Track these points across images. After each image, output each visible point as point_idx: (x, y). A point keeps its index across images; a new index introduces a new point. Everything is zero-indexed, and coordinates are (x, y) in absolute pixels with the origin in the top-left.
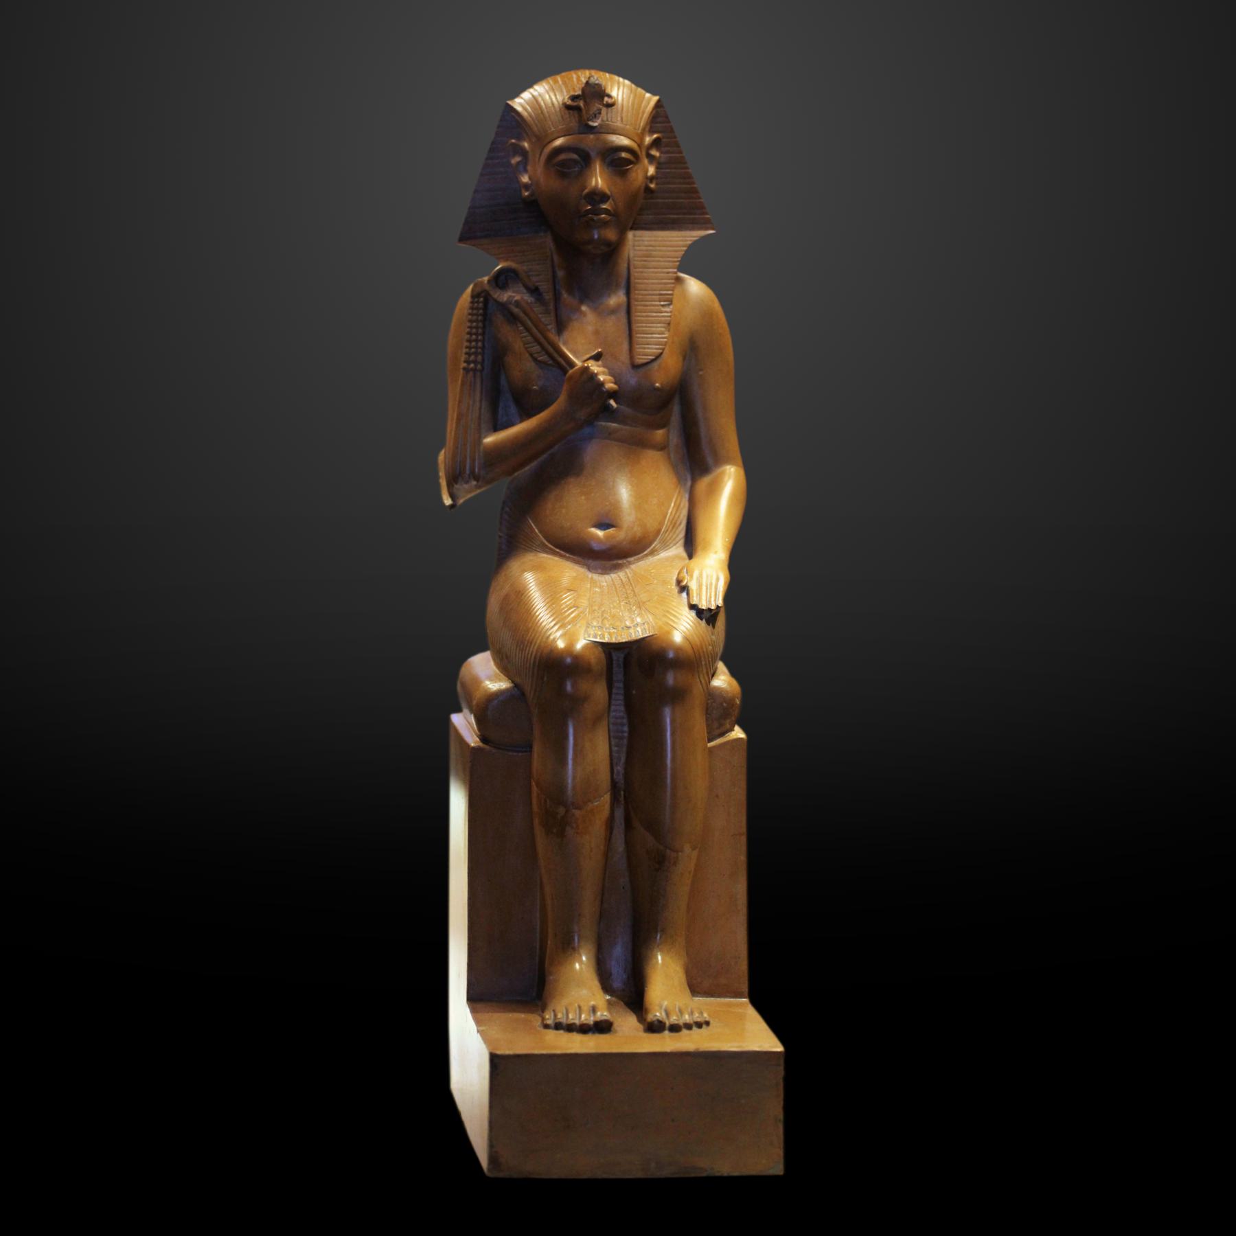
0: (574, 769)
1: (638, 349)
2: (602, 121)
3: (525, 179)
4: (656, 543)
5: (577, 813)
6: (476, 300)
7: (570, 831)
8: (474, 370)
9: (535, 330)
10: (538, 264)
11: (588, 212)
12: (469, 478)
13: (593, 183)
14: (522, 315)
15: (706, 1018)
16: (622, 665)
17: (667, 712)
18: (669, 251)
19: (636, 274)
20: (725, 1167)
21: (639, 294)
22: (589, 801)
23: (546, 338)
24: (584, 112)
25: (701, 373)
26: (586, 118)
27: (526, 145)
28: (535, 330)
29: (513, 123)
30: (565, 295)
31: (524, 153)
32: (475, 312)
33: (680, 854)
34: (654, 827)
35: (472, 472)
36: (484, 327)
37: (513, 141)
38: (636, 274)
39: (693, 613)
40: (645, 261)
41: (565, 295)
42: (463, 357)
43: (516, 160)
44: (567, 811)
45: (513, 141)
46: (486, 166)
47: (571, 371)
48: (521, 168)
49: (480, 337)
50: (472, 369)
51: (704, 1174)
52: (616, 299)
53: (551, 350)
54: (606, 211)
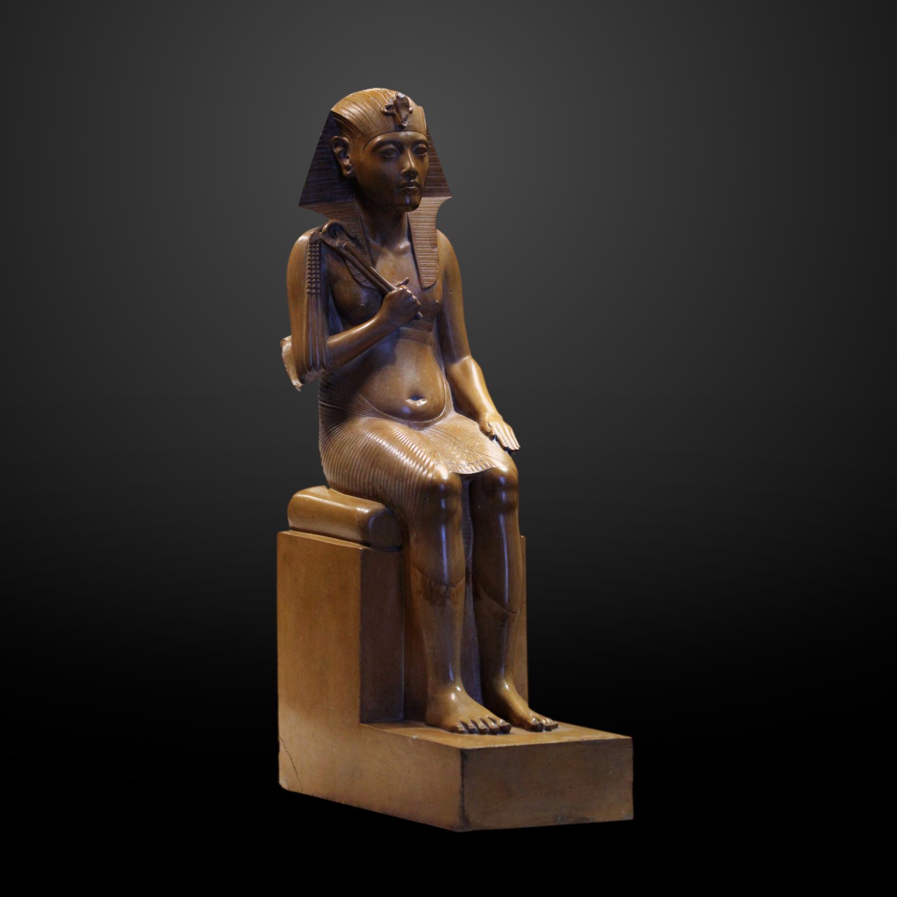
0: (448, 561)
1: (424, 277)
2: (408, 123)
3: (347, 162)
4: (444, 409)
5: (453, 589)
6: (314, 245)
7: (448, 602)
8: (316, 294)
9: (361, 266)
10: (353, 221)
11: (405, 185)
12: (320, 367)
13: (408, 165)
14: (350, 255)
15: (532, 720)
16: (468, 490)
17: (502, 519)
18: (429, 211)
19: (414, 227)
20: (600, 817)
21: (417, 240)
22: (459, 581)
24: (398, 116)
25: (451, 293)
26: (401, 121)
27: (346, 139)
28: (361, 266)
29: (338, 124)
30: (372, 241)
31: (345, 146)
32: (313, 254)
33: (516, 614)
35: (322, 363)
37: (336, 137)
38: (414, 227)
39: (506, 453)
40: (417, 218)
41: (372, 241)
42: (307, 285)
43: (338, 150)
44: (447, 589)
45: (336, 137)
46: (316, 154)
47: (390, 293)
48: (342, 155)
49: (318, 271)
50: (314, 293)
51: (589, 822)
52: (404, 244)
53: (373, 278)
54: (415, 184)
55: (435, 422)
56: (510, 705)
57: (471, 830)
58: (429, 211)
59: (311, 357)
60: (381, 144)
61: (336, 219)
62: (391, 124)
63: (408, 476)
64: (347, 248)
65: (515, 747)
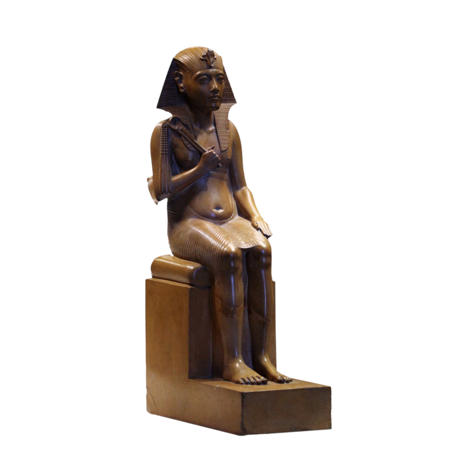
0: (235, 294)
1: (222, 145)
2: (214, 64)
3: (182, 85)
4: (233, 214)
5: (237, 309)
6: (164, 129)
7: (235, 316)
8: (166, 154)
9: (189, 139)
10: (185, 116)
11: (212, 97)
12: (168, 192)
13: (214, 87)
14: (183, 134)
15: (279, 377)
16: (245, 257)
17: (263, 272)
18: (225, 110)
19: (217, 119)
21: (219, 126)
22: (240, 304)
24: (208, 61)
25: (236, 154)
26: (210, 64)
27: (181, 73)
28: (189, 139)
30: (195, 126)
31: (181, 76)
32: (164, 133)
33: (270, 322)
34: (261, 313)
35: (169, 190)
36: (168, 139)
37: (176, 72)
38: (217, 119)
39: (265, 237)
40: (219, 114)
41: (195, 126)
42: (161, 149)
43: (177, 79)
44: (234, 308)
45: (176, 72)
47: (204, 154)
48: (179, 81)
49: (167, 142)
50: (165, 154)
52: (212, 128)
53: (196, 146)
54: (218, 96)
55: (228, 221)
56: (267, 369)
58: (225, 110)
59: (163, 187)
60: (200, 75)
61: (176, 115)
62: (205, 65)
63: (214, 249)
64: (182, 130)
65: (270, 391)
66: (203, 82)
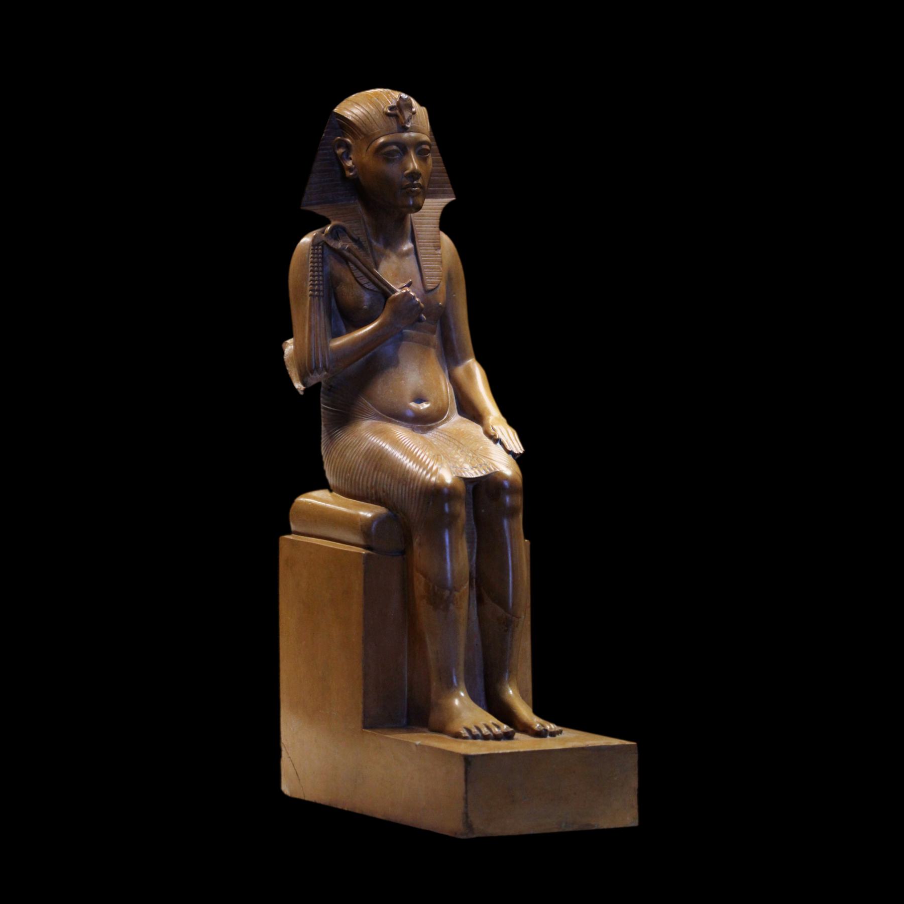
0: (452, 566)
1: (427, 280)
2: (412, 124)
3: (350, 163)
4: (448, 412)
5: (457, 594)
6: (316, 247)
7: (452, 607)
8: (319, 296)
9: (363, 268)
10: (356, 222)
11: (408, 186)
12: (323, 370)
13: (411, 167)
14: (353, 257)
16: (471, 494)
17: (506, 523)
18: (433, 212)
19: (417, 228)
20: (605, 823)
21: (421, 242)
22: (462, 585)
23: (373, 273)
24: (401, 117)
25: (454, 295)
26: (404, 122)
27: (348, 140)
28: (363, 268)
30: (375, 243)
31: (348, 147)
32: (316, 256)
33: (520, 619)
35: (324, 366)
37: (339, 138)
38: (417, 228)
39: (510, 457)
40: (421, 219)
41: (375, 243)
42: (309, 287)
43: (340, 151)
44: (451, 593)
45: (339, 138)
47: (393, 295)
48: (344, 156)
49: (320, 273)
50: (317, 296)
51: (594, 828)
52: (408, 246)
53: (376, 280)
54: (419, 185)
55: (438, 425)
56: (514, 711)
57: (474, 836)
58: (433, 212)
59: (313, 360)
60: (384, 145)
61: (339, 220)
62: (394, 125)
63: (411, 480)
64: (349, 250)
65: (519, 753)
66: (390, 157)
